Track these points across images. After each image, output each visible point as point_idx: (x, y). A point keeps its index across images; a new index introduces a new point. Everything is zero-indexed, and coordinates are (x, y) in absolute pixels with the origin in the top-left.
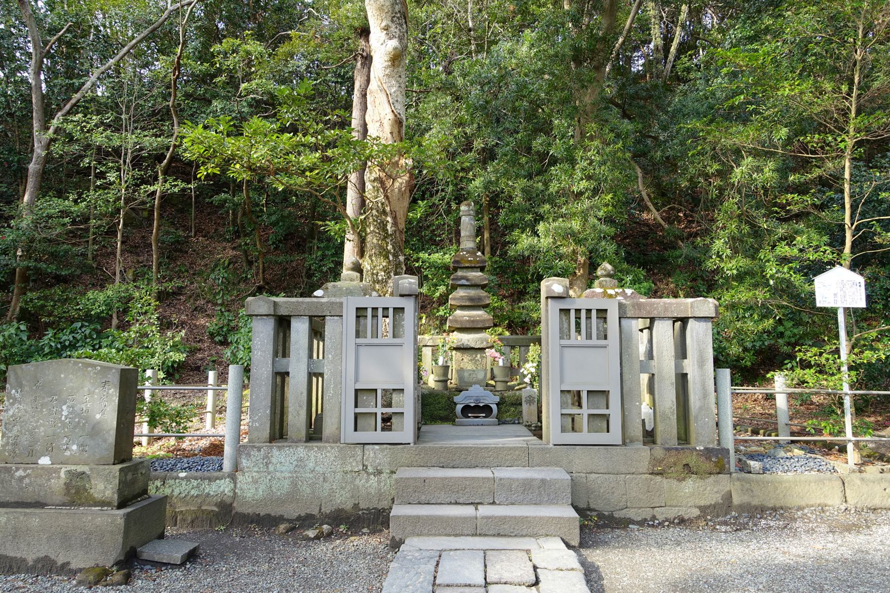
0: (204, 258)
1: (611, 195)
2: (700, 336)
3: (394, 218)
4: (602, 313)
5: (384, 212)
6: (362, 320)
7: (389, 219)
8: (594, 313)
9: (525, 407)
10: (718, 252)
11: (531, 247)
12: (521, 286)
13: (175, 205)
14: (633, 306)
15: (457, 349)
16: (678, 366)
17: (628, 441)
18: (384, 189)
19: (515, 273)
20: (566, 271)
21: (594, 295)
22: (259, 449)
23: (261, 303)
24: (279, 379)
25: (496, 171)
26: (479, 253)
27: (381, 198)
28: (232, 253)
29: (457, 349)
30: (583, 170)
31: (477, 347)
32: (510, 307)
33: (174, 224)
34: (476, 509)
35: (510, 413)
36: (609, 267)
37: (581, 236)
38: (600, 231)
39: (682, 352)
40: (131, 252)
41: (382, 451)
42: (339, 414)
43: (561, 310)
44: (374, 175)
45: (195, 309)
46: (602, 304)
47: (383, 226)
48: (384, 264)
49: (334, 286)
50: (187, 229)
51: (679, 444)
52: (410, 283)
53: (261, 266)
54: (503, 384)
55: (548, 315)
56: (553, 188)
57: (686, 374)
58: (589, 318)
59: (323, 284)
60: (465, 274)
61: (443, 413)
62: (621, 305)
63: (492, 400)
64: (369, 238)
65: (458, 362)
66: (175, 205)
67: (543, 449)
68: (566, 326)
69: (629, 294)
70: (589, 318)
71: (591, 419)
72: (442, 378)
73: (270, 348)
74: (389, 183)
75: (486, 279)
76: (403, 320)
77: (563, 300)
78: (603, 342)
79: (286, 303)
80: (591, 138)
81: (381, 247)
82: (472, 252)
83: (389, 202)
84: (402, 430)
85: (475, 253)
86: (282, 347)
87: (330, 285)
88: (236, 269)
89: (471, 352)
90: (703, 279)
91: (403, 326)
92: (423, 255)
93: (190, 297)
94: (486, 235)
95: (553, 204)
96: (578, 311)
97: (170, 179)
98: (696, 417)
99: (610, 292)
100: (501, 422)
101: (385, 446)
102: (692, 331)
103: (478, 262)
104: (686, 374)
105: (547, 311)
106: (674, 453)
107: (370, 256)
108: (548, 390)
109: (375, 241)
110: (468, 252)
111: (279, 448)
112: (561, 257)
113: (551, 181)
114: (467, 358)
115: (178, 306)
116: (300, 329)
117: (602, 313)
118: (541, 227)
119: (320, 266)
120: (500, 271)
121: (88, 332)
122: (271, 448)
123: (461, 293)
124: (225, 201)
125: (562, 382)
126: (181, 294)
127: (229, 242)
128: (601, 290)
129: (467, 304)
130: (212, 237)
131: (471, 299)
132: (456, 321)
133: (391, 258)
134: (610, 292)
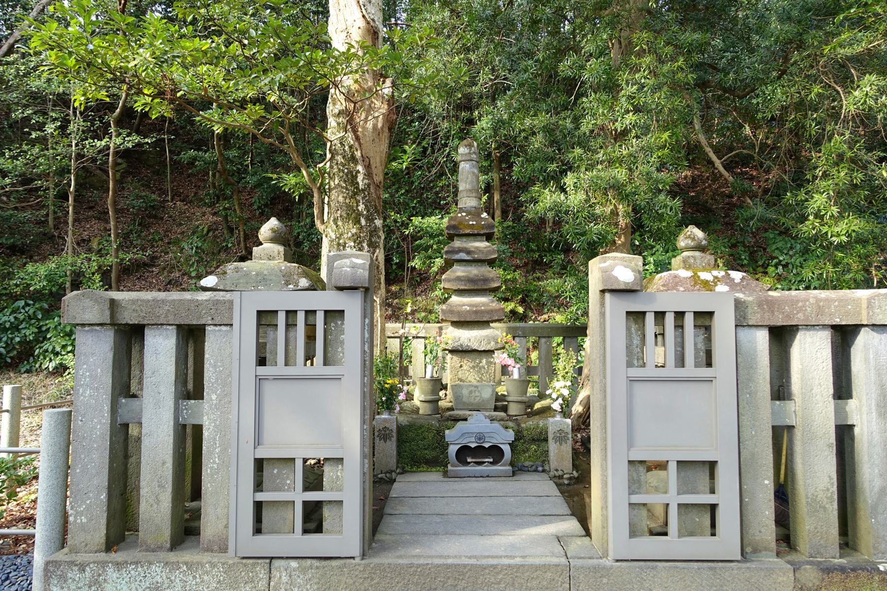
0: (181, 224)
1: (668, 133)
3: (368, 167)
4: (704, 318)
5: (353, 159)
8: (689, 320)
9: (552, 446)
10: (819, 211)
11: (556, 208)
12: (536, 255)
13: (152, 166)
14: (760, 305)
15: (453, 351)
16: (840, 412)
17: (748, 550)
19: (529, 241)
20: (604, 238)
21: (676, 282)
22: (82, 568)
23: (88, 303)
25: (509, 106)
26: (485, 215)
27: (350, 138)
28: (212, 219)
29: (453, 351)
30: (630, 98)
32: (523, 279)
33: (150, 188)
35: (530, 453)
36: (699, 233)
37: (629, 189)
38: (657, 181)
40: (99, 219)
41: (304, 570)
43: (628, 313)
44: (339, 107)
45: (170, 283)
46: (694, 302)
47: (351, 178)
48: (354, 231)
49: (237, 270)
50: (163, 192)
52: (354, 266)
53: (242, 233)
55: (605, 320)
56: (586, 126)
57: (851, 427)
59: (220, 263)
60: (465, 245)
61: (429, 454)
63: (503, 437)
65: (454, 371)
66: (152, 166)
67: (596, 569)
68: (636, 341)
69: (737, 280)
71: (683, 511)
72: (430, 398)
73: (107, 380)
75: (493, 252)
76: (342, 332)
77: (632, 295)
78: (705, 372)
79: (134, 302)
80: (641, 54)
81: (348, 207)
82: (475, 213)
83: (360, 144)
84: (340, 532)
85: (479, 215)
86: (125, 384)
87: (231, 267)
88: (215, 237)
89: (473, 356)
90: (745, 246)
91: (342, 342)
92: (417, 220)
93: (164, 269)
94: (497, 197)
95: (586, 148)
96: (660, 316)
97: (124, 132)
98: (874, 508)
99: (705, 276)
100: (517, 469)
101: (309, 562)
102: (866, 348)
103: (483, 227)
104: (851, 427)
105: (603, 314)
106: (837, 577)
107: (335, 221)
108: (605, 458)
109: (341, 199)
110: (469, 213)
111: (118, 565)
112: (595, 218)
113: (583, 116)
115: (150, 279)
116: (160, 351)
117: (704, 318)
118: (569, 180)
119: (309, 235)
120: (513, 238)
121: (31, 312)
122: (103, 564)
123: (459, 271)
124: (195, 159)
125: (630, 445)
126: (154, 266)
127: (210, 207)
128: (688, 274)
130: (191, 202)
132: (451, 312)
133: (363, 222)
134: (705, 276)
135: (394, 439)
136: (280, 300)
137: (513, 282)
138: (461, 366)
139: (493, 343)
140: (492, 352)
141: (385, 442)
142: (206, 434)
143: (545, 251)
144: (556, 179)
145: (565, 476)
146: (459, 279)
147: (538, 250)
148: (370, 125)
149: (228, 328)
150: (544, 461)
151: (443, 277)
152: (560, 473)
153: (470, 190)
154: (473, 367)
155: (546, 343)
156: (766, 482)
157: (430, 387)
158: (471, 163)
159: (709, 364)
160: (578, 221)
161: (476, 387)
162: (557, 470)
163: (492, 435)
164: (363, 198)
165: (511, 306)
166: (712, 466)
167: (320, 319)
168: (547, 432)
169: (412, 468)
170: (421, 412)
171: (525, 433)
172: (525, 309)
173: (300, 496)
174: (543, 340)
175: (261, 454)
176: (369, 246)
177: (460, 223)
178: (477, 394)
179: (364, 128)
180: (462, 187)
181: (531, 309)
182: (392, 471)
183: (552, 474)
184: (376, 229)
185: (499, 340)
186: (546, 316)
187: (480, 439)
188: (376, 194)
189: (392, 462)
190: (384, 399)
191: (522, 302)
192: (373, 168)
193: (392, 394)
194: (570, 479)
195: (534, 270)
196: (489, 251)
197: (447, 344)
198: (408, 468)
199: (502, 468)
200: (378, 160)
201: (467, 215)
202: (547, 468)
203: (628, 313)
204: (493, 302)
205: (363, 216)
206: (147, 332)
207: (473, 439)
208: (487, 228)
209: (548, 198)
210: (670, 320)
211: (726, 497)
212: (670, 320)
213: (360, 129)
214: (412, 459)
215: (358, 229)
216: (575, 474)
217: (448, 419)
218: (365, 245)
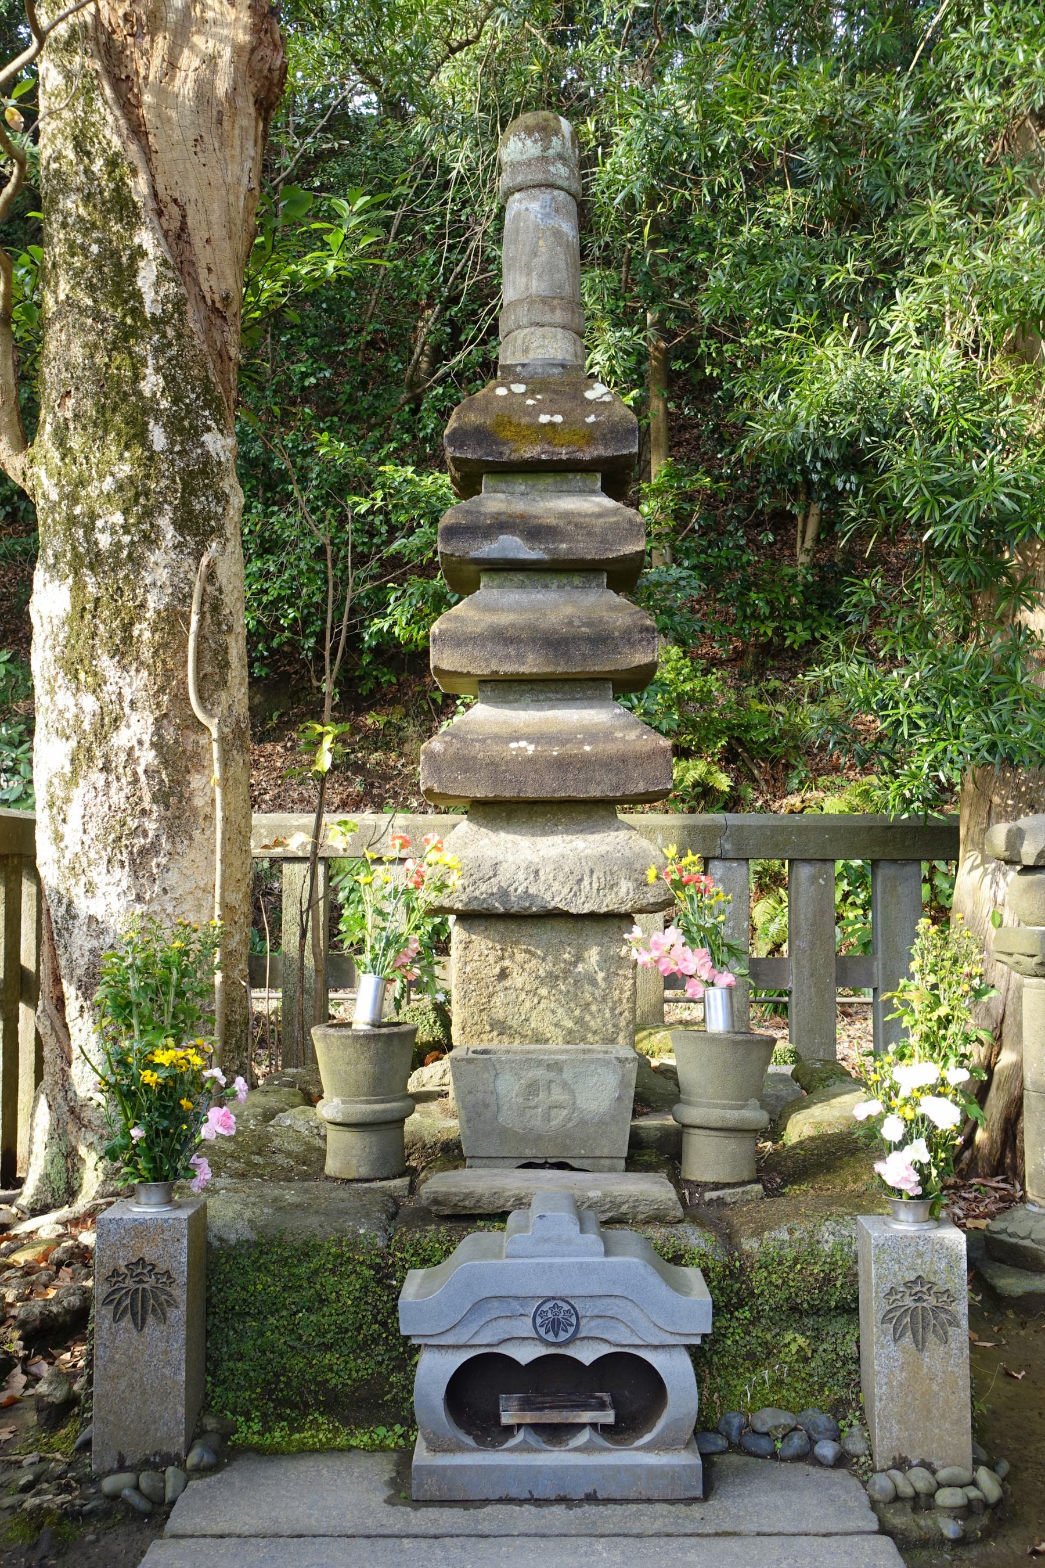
3: (178, 237)
5: (122, 206)
7: (145, 238)
9: (884, 1359)
15: (469, 917)
18: (117, 83)
27: (111, 134)
31: (582, 906)
47: (116, 275)
48: (125, 470)
54: (732, 1145)
56: (975, 108)
60: (519, 506)
61: (344, 1369)
63: (662, 1317)
64: (55, 340)
74: (148, 61)
79: (223, 809)
81: (103, 381)
83: (148, 153)
89: (548, 933)
100: (725, 1450)
103: (591, 435)
109: (77, 353)
110: (537, 384)
114: (527, 963)
118: (904, 313)
129: (531, 664)
131: (555, 643)
132: (465, 763)
133: (158, 438)
135: (178, 1314)
137: (702, 702)
138: (503, 975)
139: (625, 886)
140: (623, 919)
141: (140, 1325)
143: (792, 617)
144: (858, 307)
145: (946, 1497)
146: (502, 637)
147: (772, 617)
148: (184, 85)
150: (838, 1409)
151: (435, 628)
152: (920, 1480)
153: (544, 300)
154: (552, 979)
155: (813, 879)
157: (364, 1066)
158: (546, 195)
160: (940, 446)
161: (555, 1067)
162: (901, 1464)
163: (613, 1307)
164: (158, 351)
165: (694, 771)
168: (852, 1279)
169: (267, 1429)
170: (332, 1166)
171: (758, 1278)
172: (737, 781)
174: (805, 871)
176: (180, 526)
177: (504, 422)
178: (558, 1095)
179: (161, 93)
180: (513, 288)
181: (754, 780)
182: (168, 1460)
183: (882, 1483)
184: (207, 467)
185: (651, 874)
186: (794, 800)
187: (555, 1326)
188: (210, 341)
189: (170, 1421)
190: (137, 1133)
191: (729, 759)
192: (197, 241)
193: (176, 1115)
194: (967, 1511)
195: (760, 671)
196: (614, 528)
197: (442, 887)
198: (249, 1432)
199: (657, 1456)
200: (217, 214)
201: (530, 393)
202: (855, 1445)
204: (629, 727)
205: (158, 414)
207: (524, 1327)
208: (605, 441)
209: (836, 366)
213: (147, 98)
214: (268, 1391)
215: (138, 462)
216: (989, 1485)
217: (425, 1215)
218: (165, 522)
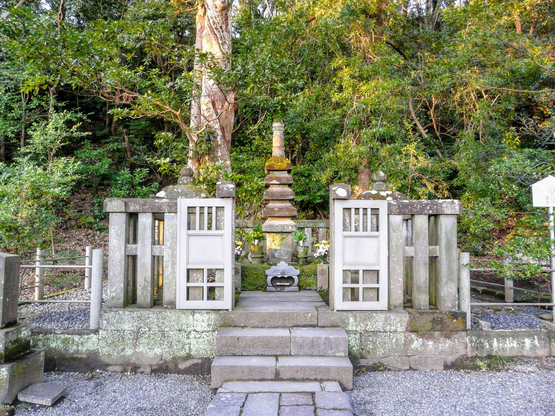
2: (448, 225)
4: (375, 211)
6: (192, 216)
8: (369, 211)
24: (130, 260)
34: (277, 360)
39: (434, 239)
42: (176, 286)
51: (430, 309)
58: (365, 214)
62: (389, 205)
63: (294, 272)
70: (365, 214)
78: (376, 233)
86: (132, 236)
116: (145, 220)
135: (240, 274)
136: (197, 202)
142: (165, 259)
149: (174, 214)
156: (400, 279)
159: (378, 230)
166: (378, 272)
167: (214, 210)
173: (206, 285)
175: (190, 267)
203: (344, 209)
206: (139, 215)
207: (279, 273)
210: (361, 211)
211: (383, 285)
212: (361, 211)
